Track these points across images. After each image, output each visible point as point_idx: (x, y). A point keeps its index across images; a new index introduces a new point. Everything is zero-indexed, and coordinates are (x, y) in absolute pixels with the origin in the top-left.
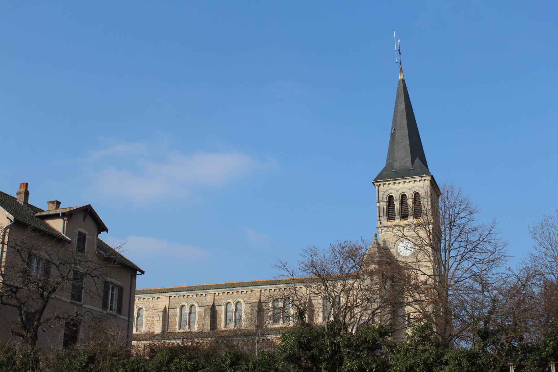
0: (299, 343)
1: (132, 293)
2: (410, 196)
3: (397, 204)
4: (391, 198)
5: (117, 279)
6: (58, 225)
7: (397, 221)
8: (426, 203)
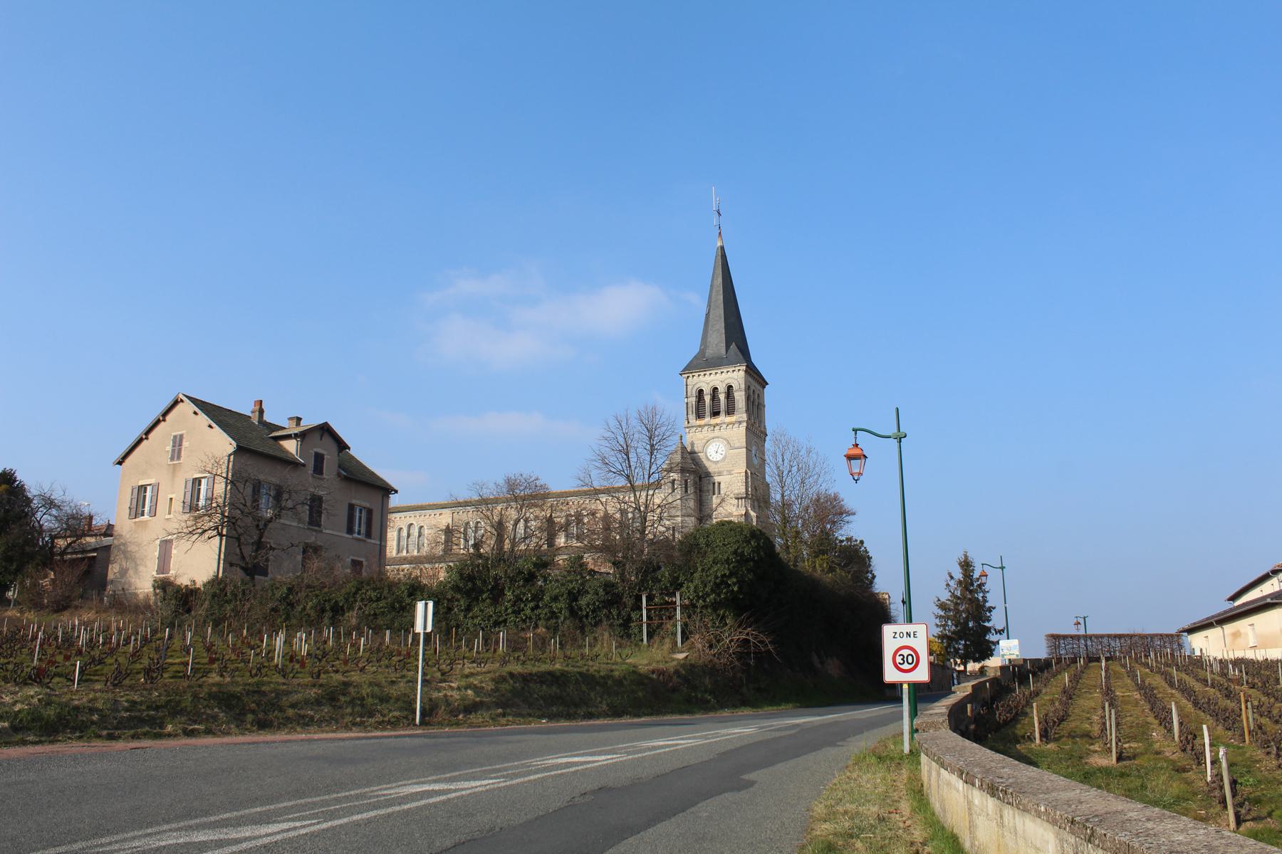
0: (461, 575)
1: (385, 511)
2: (722, 389)
3: (707, 399)
4: (701, 392)
5: (362, 500)
6: (291, 446)
7: (707, 420)
8: (740, 397)
